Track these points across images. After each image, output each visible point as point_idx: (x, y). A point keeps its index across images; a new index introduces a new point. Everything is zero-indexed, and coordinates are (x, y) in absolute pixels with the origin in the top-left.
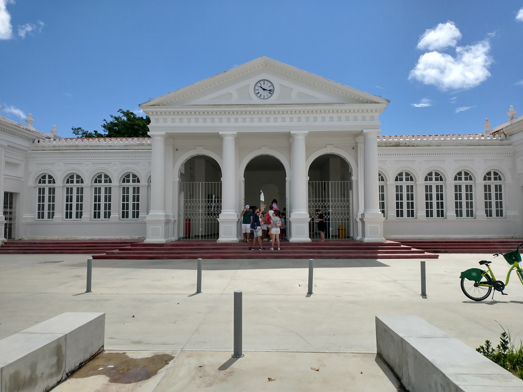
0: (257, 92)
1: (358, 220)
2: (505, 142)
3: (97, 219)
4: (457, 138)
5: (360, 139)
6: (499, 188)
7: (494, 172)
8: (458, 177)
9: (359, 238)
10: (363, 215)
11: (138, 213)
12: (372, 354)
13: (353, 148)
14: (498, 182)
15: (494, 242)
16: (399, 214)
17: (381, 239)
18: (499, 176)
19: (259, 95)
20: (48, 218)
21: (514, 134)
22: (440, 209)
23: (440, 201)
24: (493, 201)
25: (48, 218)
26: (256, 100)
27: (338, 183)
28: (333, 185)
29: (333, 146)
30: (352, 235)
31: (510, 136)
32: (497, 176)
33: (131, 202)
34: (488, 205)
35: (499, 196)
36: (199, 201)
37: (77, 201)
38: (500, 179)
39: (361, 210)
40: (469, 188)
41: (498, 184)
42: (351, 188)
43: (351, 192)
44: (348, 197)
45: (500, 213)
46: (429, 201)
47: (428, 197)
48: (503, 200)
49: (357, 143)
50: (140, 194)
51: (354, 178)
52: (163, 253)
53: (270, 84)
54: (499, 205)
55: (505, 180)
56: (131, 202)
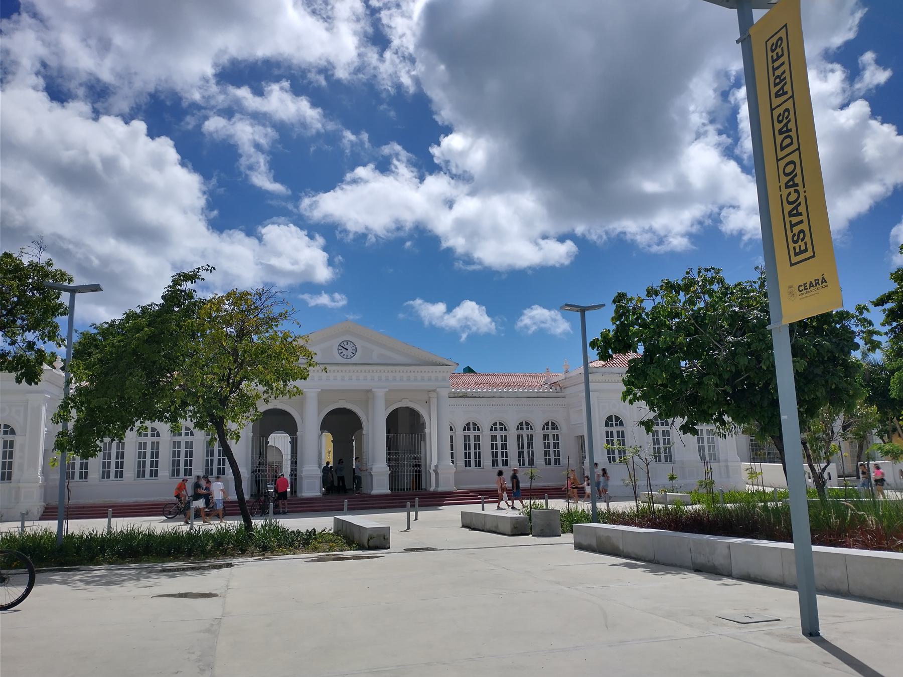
0: (340, 351)
1: (431, 471)
2: (560, 394)
3: (119, 479)
4: (498, 389)
5: (433, 395)
6: (556, 437)
7: (526, 422)
8: (493, 427)
9: (432, 489)
10: (436, 466)
11: (156, 471)
12: (754, 571)
13: (426, 402)
14: (555, 432)
15: (549, 489)
16: (467, 464)
17: (454, 489)
18: (505, 426)
19: (342, 355)
20: (80, 479)
21: (568, 387)
22: (557, 457)
23: (521, 450)
24: (552, 450)
25: (80, 479)
26: (339, 359)
27: (406, 435)
28: (404, 438)
29: (408, 400)
30: (423, 487)
31: (564, 388)
32: (555, 427)
33: (472, 451)
34: (547, 454)
35: (556, 445)
36: (404, 453)
37: (152, 457)
38: (557, 429)
39: (435, 462)
40: (530, 438)
41: (9, 440)
42: (425, 440)
43: (423, 443)
44: (419, 448)
45: (558, 462)
46: (556, 450)
47: (494, 447)
48: (560, 449)
49: (430, 397)
50: (125, 451)
51: (427, 431)
52: (376, 504)
53: (352, 345)
54: (557, 454)
55: (561, 431)
56: (472, 451)
